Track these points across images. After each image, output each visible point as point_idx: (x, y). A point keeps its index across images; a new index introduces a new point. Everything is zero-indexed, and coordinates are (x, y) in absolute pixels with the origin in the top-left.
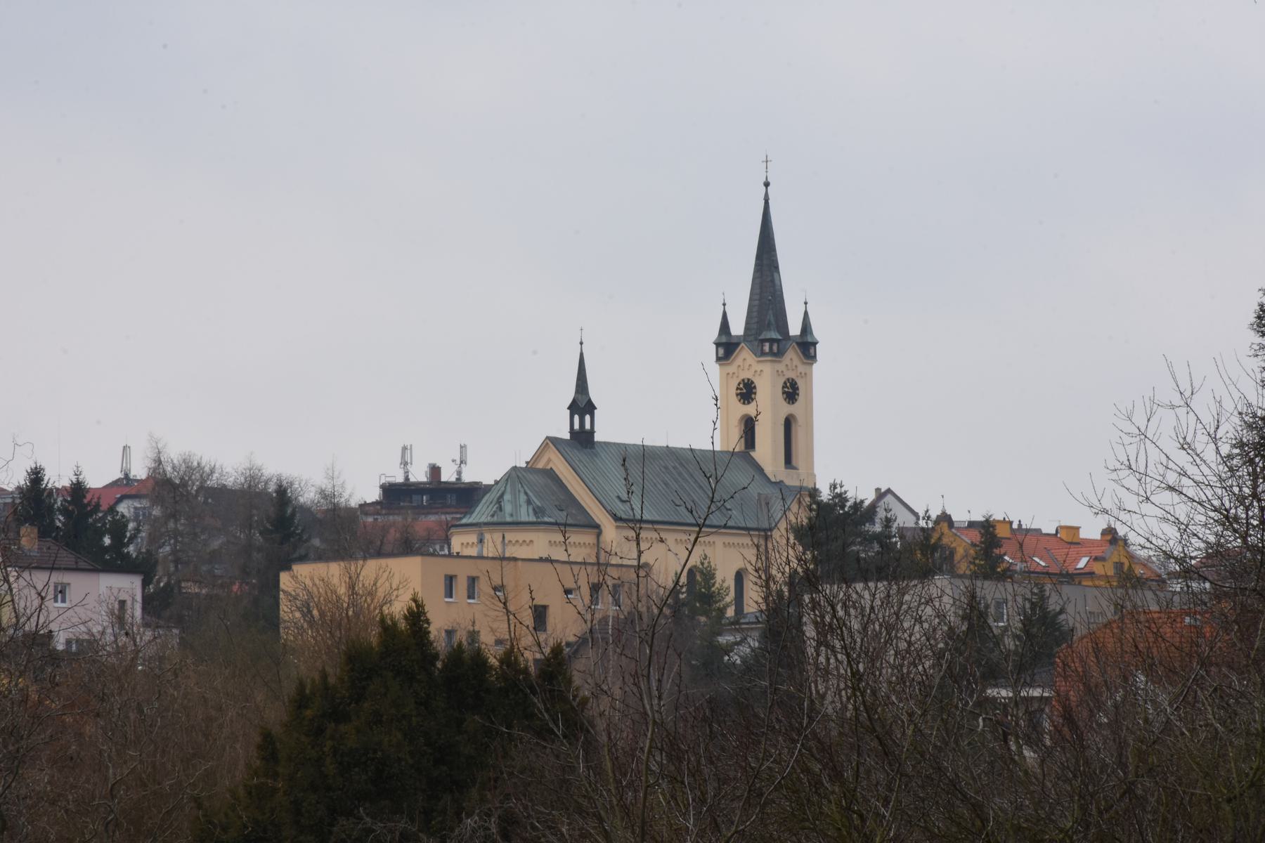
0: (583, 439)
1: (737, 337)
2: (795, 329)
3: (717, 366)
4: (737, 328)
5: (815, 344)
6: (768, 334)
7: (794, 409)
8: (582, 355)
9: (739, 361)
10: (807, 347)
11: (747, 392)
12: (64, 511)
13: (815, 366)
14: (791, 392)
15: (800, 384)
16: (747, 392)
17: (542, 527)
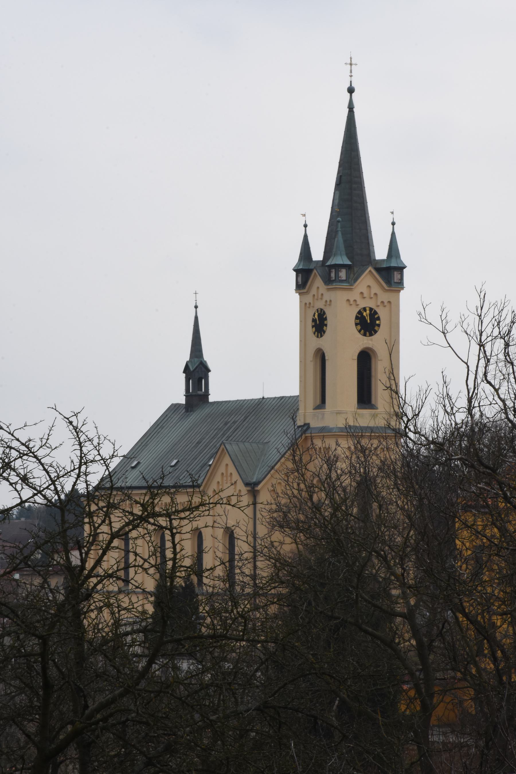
2: (381, 252)
3: (297, 296)
4: (318, 254)
5: (401, 269)
6: (348, 264)
7: (376, 342)
8: (196, 318)
9: (314, 291)
10: (391, 273)
13: (403, 294)
14: (368, 323)
15: (382, 313)
16: (319, 324)
17: (369, 369)
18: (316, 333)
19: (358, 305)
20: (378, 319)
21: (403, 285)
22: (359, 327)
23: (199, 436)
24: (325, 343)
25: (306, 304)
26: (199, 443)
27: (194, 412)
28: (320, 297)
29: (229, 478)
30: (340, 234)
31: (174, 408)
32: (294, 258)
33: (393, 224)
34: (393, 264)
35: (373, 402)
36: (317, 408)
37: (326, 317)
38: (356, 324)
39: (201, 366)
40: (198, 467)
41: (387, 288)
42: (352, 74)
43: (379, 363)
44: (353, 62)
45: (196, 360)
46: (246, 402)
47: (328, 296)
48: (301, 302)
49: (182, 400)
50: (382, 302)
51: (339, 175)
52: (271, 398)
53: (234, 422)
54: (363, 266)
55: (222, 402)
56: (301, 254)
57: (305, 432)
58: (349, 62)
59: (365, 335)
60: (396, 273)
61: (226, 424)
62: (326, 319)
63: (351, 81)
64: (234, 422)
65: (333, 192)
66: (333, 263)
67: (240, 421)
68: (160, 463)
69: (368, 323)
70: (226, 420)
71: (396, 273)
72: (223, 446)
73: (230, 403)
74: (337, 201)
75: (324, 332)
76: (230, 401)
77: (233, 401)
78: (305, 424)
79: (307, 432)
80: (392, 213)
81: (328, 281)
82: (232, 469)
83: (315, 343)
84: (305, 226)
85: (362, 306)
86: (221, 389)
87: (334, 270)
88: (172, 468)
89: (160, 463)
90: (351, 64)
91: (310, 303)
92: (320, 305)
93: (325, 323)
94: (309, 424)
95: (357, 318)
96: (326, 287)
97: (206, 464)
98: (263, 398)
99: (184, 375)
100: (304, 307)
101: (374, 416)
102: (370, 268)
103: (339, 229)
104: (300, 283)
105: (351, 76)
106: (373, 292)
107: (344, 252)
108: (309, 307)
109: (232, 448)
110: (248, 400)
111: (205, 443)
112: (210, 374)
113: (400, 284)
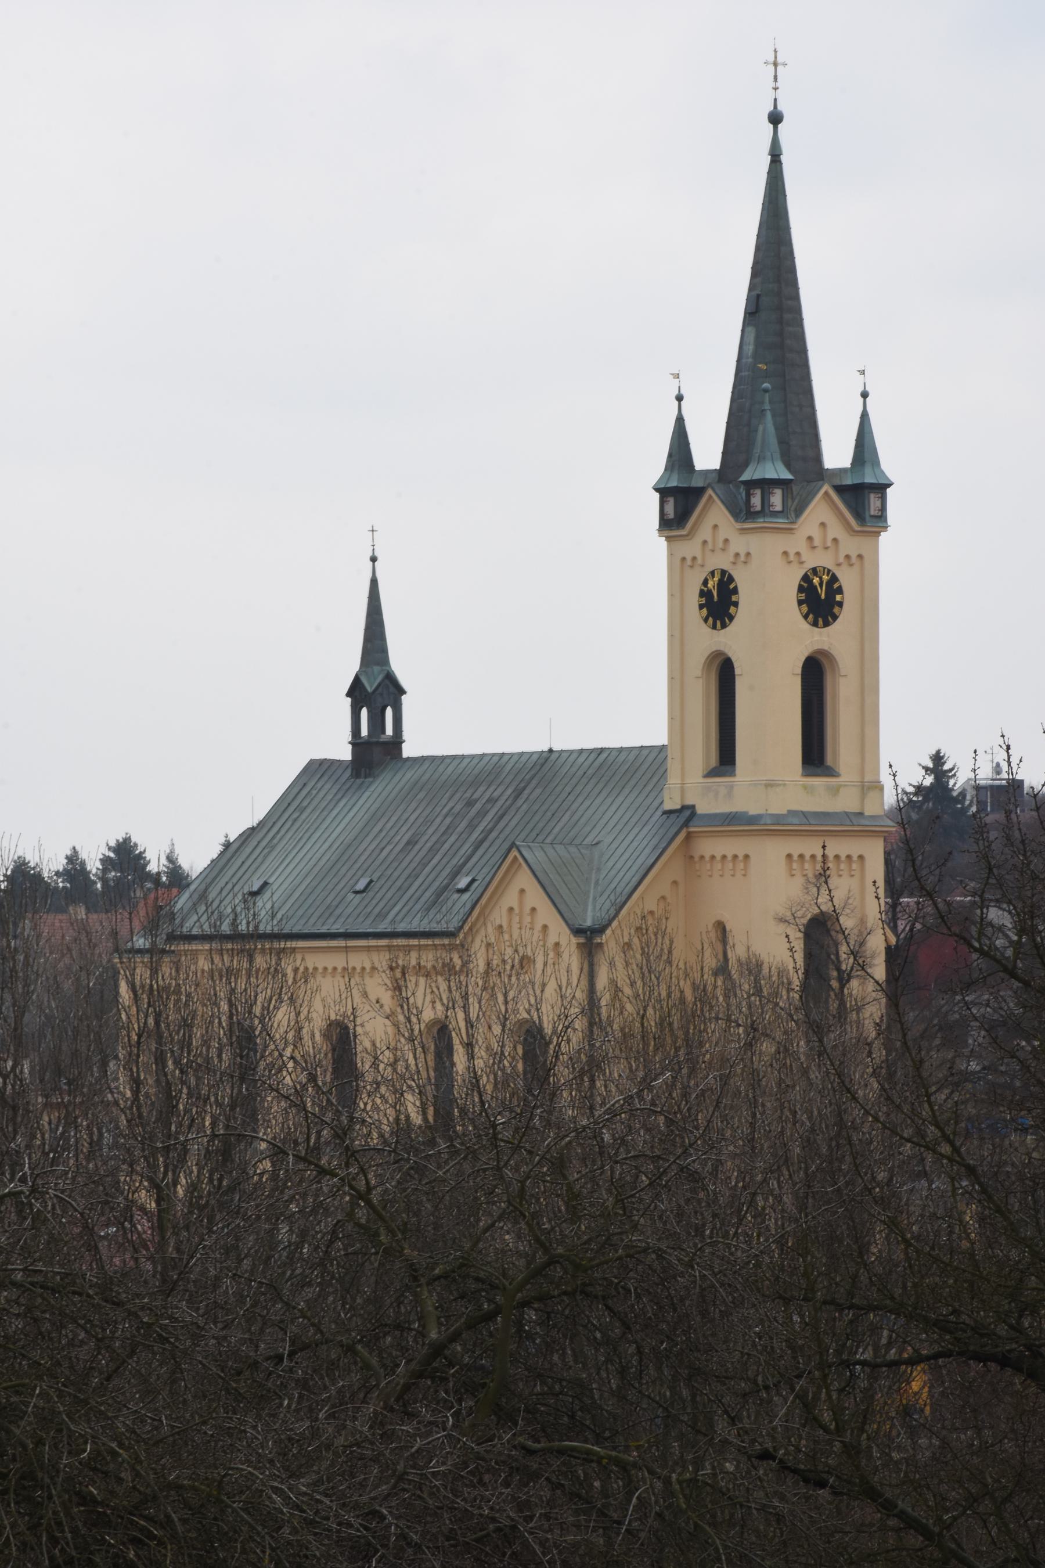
0: (376, 751)
1: (706, 473)
2: (837, 452)
3: (662, 542)
4: (708, 455)
5: (881, 488)
6: (769, 475)
7: (834, 639)
8: (374, 582)
9: (705, 532)
10: (863, 496)
11: (719, 603)
12: (295, 1101)
13: (884, 537)
14: (820, 601)
15: (847, 579)
16: (719, 603)
18: (710, 619)
19: (802, 563)
20: (840, 591)
21: (886, 521)
22: (805, 608)
23: (404, 829)
24: (732, 639)
25: (684, 559)
26: (411, 843)
27: (375, 777)
28: (721, 545)
29: (527, 919)
30: (769, 416)
31: (318, 770)
32: (655, 464)
33: (865, 395)
34: (869, 479)
35: (829, 761)
36: (711, 773)
37: (736, 588)
38: (800, 603)
39: (387, 682)
40: (428, 894)
41: (857, 528)
42: (778, 85)
43: (842, 681)
44: (779, 60)
45: (376, 669)
46: (505, 758)
47: (740, 543)
48: (671, 555)
49: (344, 753)
50: (848, 557)
51: (755, 293)
52: (572, 751)
53: (492, 801)
54: (809, 482)
55: (443, 758)
56: (670, 455)
57: (686, 824)
58: (772, 59)
59: (815, 624)
60: (872, 496)
61: (470, 804)
62: (735, 591)
63: (775, 100)
64: (492, 801)
65: (740, 328)
66: (757, 476)
67: (505, 797)
68: (324, 884)
69: (820, 601)
70: (468, 795)
71: (872, 496)
72: (514, 853)
73: (466, 761)
74: (750, 349)
75: (731, 618)
76: (463, 757)
77: (473, 757)
78: (684, 808)
79: (691, 823)
80: (863, 372)
81: (743, 513)
82: (535, 897)
83: (707, 640)
84: (680, 398)
85: (810, 564)
86: (428, 731)
87: (758, 492)
88: (466, 896)
89: (324, 884)
90: (775, 64)
91: (694, 559)
92: (720, 561)
93: (734, 598)
94: (693, 807)
95: (801, 589)
96: (739, 526)
97: (448, 885)
98: (551, 751)
99: (349, 700)
100: (679, 566)
101: (835, 791)
102: (826, 487)
103: (767, 406)
104: (671, 516)
105: (776, 89)
106: (831, 535)
107: (777, 455)
108: (691, 567)
109: (536, 855)
110: (512, 755)
111: (429, 845)
112: (404, 698)
113: (881, 518)
